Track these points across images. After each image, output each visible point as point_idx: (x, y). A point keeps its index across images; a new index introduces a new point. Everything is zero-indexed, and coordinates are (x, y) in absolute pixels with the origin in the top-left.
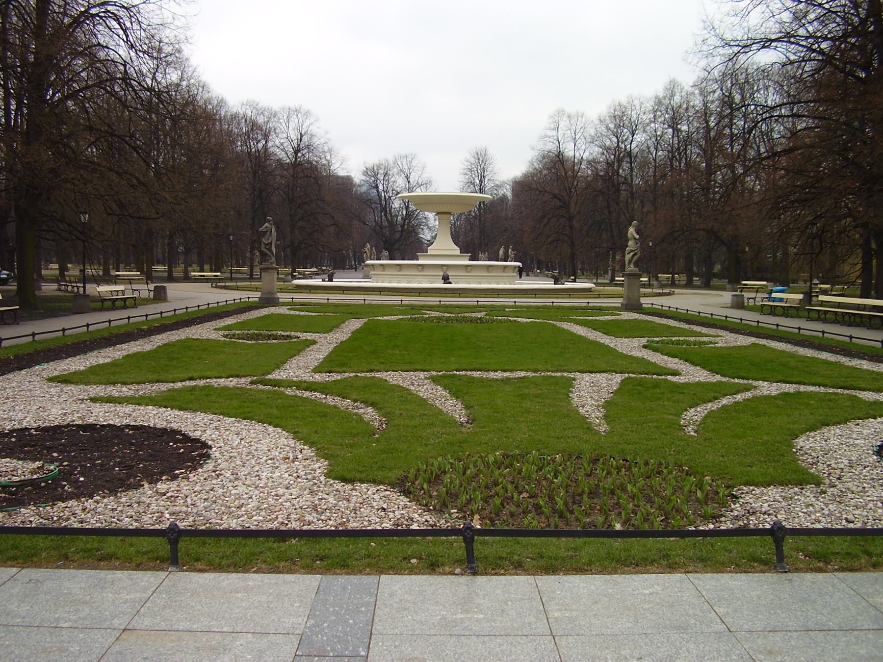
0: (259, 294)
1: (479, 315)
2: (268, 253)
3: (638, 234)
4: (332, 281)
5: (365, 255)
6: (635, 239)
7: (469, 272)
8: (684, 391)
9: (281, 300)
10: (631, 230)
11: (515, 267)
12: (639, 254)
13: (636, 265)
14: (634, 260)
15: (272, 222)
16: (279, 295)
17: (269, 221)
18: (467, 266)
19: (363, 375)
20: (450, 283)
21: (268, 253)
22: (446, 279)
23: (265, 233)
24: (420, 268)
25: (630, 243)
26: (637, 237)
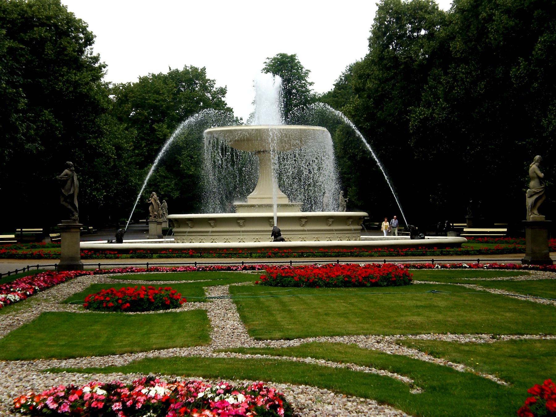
0: (58, 262)
1: (246, 284)
2: (70, 207)
3: (542, 171)
4: (122, 242)
5: (150, 208)
6: (539, 177)
7: (303, 226)
8: (191, 372)
9: (85, 267)
10: (534, 167)
11: (360, 218)
12: (544, 198)
13: (540, 211)
14: (538, 204)
15: (73, 168)
16: (84, 262)
17: (68, 167)
18: (300, 218)
19: (358, 368)
20: (282, 240)
21: (70, 207)
22: (277, 235)
23: (65, 182)
24: (212, 223)
25: (532, 184)
26: (542, 175)
